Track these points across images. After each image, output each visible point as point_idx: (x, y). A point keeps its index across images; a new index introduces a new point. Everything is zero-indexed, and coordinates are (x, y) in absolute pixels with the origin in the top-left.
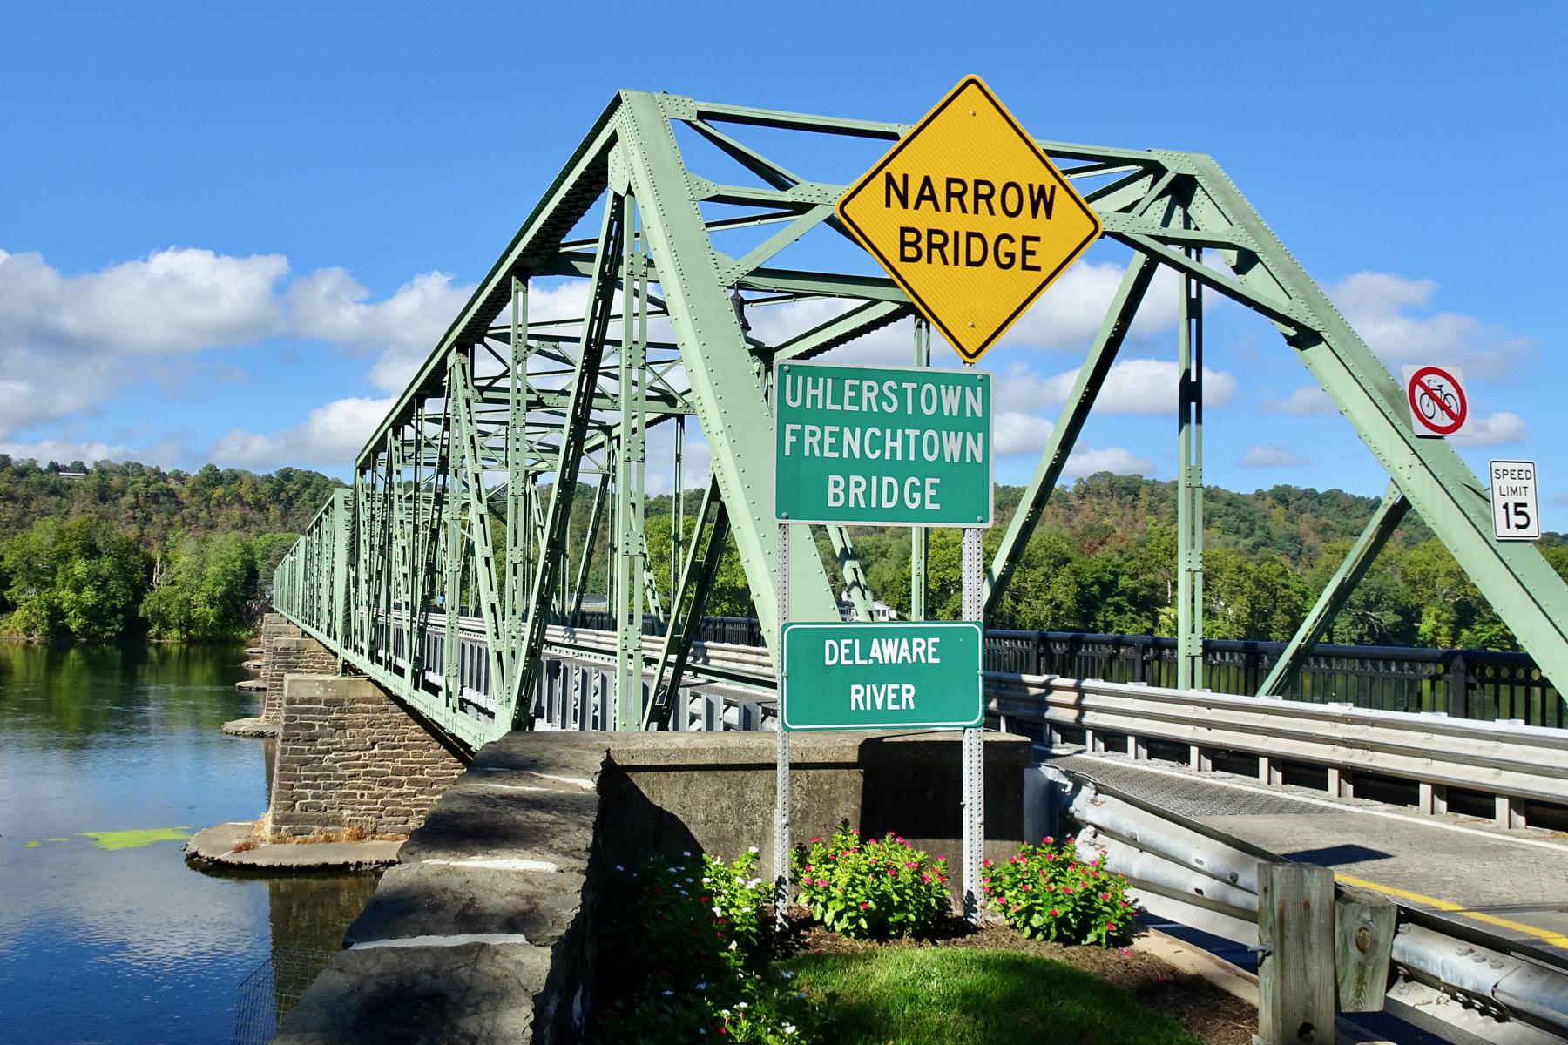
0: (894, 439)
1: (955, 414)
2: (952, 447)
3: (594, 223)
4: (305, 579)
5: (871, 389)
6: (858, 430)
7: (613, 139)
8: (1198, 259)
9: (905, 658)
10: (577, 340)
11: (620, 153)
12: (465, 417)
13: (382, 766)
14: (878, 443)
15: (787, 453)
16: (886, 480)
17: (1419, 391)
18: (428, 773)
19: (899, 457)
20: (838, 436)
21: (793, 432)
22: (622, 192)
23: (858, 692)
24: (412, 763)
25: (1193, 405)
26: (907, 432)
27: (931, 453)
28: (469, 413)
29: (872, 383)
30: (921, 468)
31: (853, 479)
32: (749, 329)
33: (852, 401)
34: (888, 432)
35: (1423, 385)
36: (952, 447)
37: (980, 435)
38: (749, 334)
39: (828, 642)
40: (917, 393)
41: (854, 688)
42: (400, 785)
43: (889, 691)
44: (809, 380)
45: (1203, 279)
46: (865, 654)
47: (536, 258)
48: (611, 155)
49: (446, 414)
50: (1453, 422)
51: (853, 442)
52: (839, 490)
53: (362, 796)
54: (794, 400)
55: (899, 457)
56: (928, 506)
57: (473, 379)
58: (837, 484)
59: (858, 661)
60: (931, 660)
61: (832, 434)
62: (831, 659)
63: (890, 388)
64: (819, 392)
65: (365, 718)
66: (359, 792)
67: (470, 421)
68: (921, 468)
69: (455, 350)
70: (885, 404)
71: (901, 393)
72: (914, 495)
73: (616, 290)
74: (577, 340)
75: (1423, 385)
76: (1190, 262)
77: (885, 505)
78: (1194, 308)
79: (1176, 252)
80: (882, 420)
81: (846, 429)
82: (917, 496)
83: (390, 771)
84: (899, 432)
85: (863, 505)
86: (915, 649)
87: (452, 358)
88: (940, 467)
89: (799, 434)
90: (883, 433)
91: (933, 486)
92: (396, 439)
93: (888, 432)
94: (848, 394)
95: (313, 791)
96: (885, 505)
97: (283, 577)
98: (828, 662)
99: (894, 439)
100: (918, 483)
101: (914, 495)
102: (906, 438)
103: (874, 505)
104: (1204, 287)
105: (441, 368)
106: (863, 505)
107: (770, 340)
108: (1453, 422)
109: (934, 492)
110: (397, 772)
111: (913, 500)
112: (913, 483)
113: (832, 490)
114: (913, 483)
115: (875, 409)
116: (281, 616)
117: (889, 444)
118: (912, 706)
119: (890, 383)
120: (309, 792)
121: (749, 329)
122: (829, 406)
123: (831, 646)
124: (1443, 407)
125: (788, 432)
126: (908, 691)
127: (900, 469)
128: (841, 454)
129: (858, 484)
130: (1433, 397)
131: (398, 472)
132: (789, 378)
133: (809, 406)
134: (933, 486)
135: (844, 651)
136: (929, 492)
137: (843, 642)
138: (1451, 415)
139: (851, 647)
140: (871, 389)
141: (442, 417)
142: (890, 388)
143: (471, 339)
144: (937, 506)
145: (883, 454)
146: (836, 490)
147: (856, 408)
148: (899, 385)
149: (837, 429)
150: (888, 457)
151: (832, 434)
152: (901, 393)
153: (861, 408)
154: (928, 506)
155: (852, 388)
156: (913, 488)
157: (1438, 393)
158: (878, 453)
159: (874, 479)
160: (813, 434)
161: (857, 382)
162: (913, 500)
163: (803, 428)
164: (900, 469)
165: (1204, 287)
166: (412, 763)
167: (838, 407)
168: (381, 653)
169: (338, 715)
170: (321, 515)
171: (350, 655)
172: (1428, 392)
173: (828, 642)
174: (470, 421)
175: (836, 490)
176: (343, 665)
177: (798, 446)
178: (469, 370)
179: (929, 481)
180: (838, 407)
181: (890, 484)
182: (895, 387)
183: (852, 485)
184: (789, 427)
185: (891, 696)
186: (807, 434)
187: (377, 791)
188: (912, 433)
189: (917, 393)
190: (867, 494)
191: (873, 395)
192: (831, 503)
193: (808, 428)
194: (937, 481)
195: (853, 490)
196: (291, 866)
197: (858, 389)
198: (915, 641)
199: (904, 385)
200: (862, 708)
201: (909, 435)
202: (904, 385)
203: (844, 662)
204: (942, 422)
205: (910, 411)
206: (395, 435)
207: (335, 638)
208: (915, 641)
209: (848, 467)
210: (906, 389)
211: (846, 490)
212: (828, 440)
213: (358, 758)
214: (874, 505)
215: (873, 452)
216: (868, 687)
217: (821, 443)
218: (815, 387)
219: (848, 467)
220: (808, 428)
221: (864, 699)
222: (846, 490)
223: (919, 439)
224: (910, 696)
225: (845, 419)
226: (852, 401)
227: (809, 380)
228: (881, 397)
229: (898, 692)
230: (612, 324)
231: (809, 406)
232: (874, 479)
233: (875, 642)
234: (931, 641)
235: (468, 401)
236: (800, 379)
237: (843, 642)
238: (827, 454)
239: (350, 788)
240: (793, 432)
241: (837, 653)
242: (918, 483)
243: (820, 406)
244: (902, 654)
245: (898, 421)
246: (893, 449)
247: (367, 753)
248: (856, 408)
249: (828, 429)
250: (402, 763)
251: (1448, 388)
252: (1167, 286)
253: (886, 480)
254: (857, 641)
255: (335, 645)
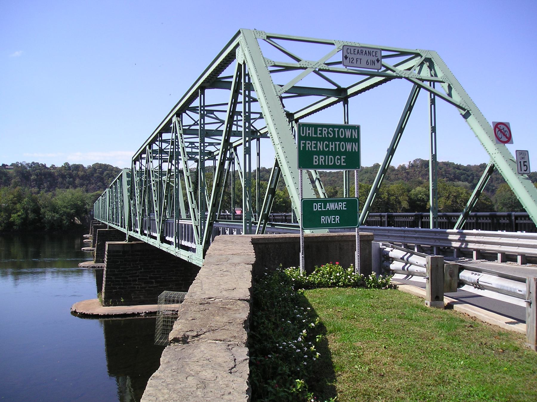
0: (332, 145)
1: (350, 137)
2: (349, 147)
3: (231, 71)
4: (109, 206)
5: (325, 130)
6: (322, 142)
7: (238, 45)
8: (434, 87)
9: (336, 208)
10: (226, 111)
11: (240, 49)
12: (180, 141)
13: (145, 276)
14: (328, 146)
15: (302, 149)
16: (330, 157)
17: (497, 130)
18: (163, 278)
19: (334, 150)
20: (316, 144)
21: (303, 143)
22: (241, 63)
23: (323, 218)
24: (156, 274)
25: (400, 134)
26: (336, 143)
27: (343, 149)
28: (182, 139)
29: (325, 129)
30: (340, 153)
31: (321, 157)
32: (285, 107)
33: (320, 134)
34: (330, 143)
35: (498, 128)
36: (349, 147)
37: (357, 143)
38: (285, 109)
39: (314, 204)
40: (338, 131)
41: (322, 217)
42: (152, 283)
43: (332, 218)
44: (307, 128)
45: (435, 94)
46: (325, 208)
47: (208, 83)
48: (237, 50)
49: (172, 139)
50: (507, 140)
51: (320, 146)
52: (317, 160)
53: (138, 288)
54: (303, 134)
55: (334, 150)
56: (342, 164)
57: (183, 126)
58: (316, 158)
59: (323, 209)
60: (344, 209)
61: (314, 144)
62: (315, 209)
63: (331, 130)
64: (310, 132)
65: (138, 258)
66: (136, 286)
67: (182, 142)
68: (340, 153)
69: (175, 116)
70: (329, 135)
71: (334, 132)
72: (338, 161)
73: (239, 95)
74: (226, 111)
75: (498, 128)
76: (431, 88)
77: (330, 164)
78: (433, 102)
79: (427, 84)
80: (329, 139)
81: (318, 142)
82: (339, 161)
83: (148, 278)
84: (334, 143)
85: (324, 164)
86: (339, 206)
87: (175, 119)
88: (345, 153)
89: (305, 144)
90: (329, 143)
91: (344, 158)
92: (150, 149)
93: (330, 143)
94: (319, 132)
95: (119, 286)
96: (330, 164)
97: (99, 206)
98: (314, 210)
99: (332, 145)
100: (339, 158)
101: (338, 161)
102: (336, 144)
103: (327, 164)
104: (436, 96)
105: (170, 121)
106: (324, 164)
107: (291, 111)
108: (507, 140)
109: (344, 160)
110: (151, 278)
111: (338, 163)
112: (338, 158)
113: (314, 160)
114: (338, 158)
115: (327, 136)
116: (96, 220)
117: (331, 146)
118: (339, 222)
119: (331, 129)
120: (118, 287)
121: (285, 107)
122: (313, 135)
123: (315, 205)
124: (504, 135)
125: (301, 143)
126: (338, 218)
127: (334, 154)
128: (317, 149)
129: (322, 158)
130: (501, 132)
131: (151, 162)
132: (301, 128)
133: (307, 135)
134: (344, 158)
135: (319, 206)
136: (343, 160)
137: (319, 204)
138: (507, 137)
139: (321, 205)
140: (325, 130)
141: (171, 141)
142: (331, 130)
143: (182, 112)
144: (345, 164)
145: (329, 149)
146: (316, 160)
147: (321, 136)
148: (333, 129)
149: (315, 142)
150: (330, 150)
151: (314, 144)
152: (334, 132)
153: (322, 136)
154: (342, 164)
155: (320, 130)
156: (338, 159)
157: (503, 131)
158: (328, 149)
159: (327, 156)
160: (309, 144)
161: (321, 129)
162: (338, 163)
163: (306, 142)
164: (334, 154)
165: (436, 96)
166: (156, 274)
167: (316, 136)
168: (146, 232)
169: (128, 257)
170: (116, 180)
171: (132, 233)
172: (500, 130)
173: (314, 204)
174: (182, 142)
175: (316, 160)
176: (129, 237)
177: (304, 147)
178: (180, 122)
179: (342, 157)
180: (316, 136)
181: (331, 158)
182: (332, 130)
183: (320, 158)
184: (302, 142)
185: (333, 219)
186: (307, 144)
187: (143, 285)
188: (337, 143)
189: (338, 131)
190: (325, 161)
191: (326, 132)
192: (314, 164)
193: (307, 142)
194: (345, 157)
195: (321, 160)
196: (112, 314)
197: (321, 131)
198: (339, 203)
199: (335, 129)
200: (324, 223)
201: (336, 144)
202: (335, 129)
203: (319, 210)
204: (346, 140)
205: (336, 137)
206: (150, 148)
207: (125, 228)
208: (339, 203)
209: (319, 153)
210: (335, 130)
211: (319, 160)
212: (313, 145)
213: (136, 273)
214: (327, 164)
215: (326, 149)
216: (326, 217)
217: (311, 146)
218: (309, 130)
219: (319, 153)
220: (307, 142)
221: (325, 220)
222: (319, 160)
223: (339, 145)
224: (338, 219)
225: (317, 139)
226: (320, 134)
227: (307, 128)
228: (328, 133)
229: (334, 218)
230: (238, 105)
231: (307, 135)
232: (327, 156)
233: (328, 203)
234: (344, 203)
235: (181, 134)
236: (305, 128)
237: (319, 204)
238: (313, 149)
239: (133, 285)
240: (303, 143)
241: (317, 207)
242: (339, 158)
243: (311, 136)
244: (335, 207)
245: (333, 139)
246: (332, 148)
247: (139, 271)
248: (321, 136)
249: (313, 142)
250: (153, 275)
251: (506, 129)
252: (424, 96)
253: (330, 157)
254: (323, 204)
255: (125, 231)
